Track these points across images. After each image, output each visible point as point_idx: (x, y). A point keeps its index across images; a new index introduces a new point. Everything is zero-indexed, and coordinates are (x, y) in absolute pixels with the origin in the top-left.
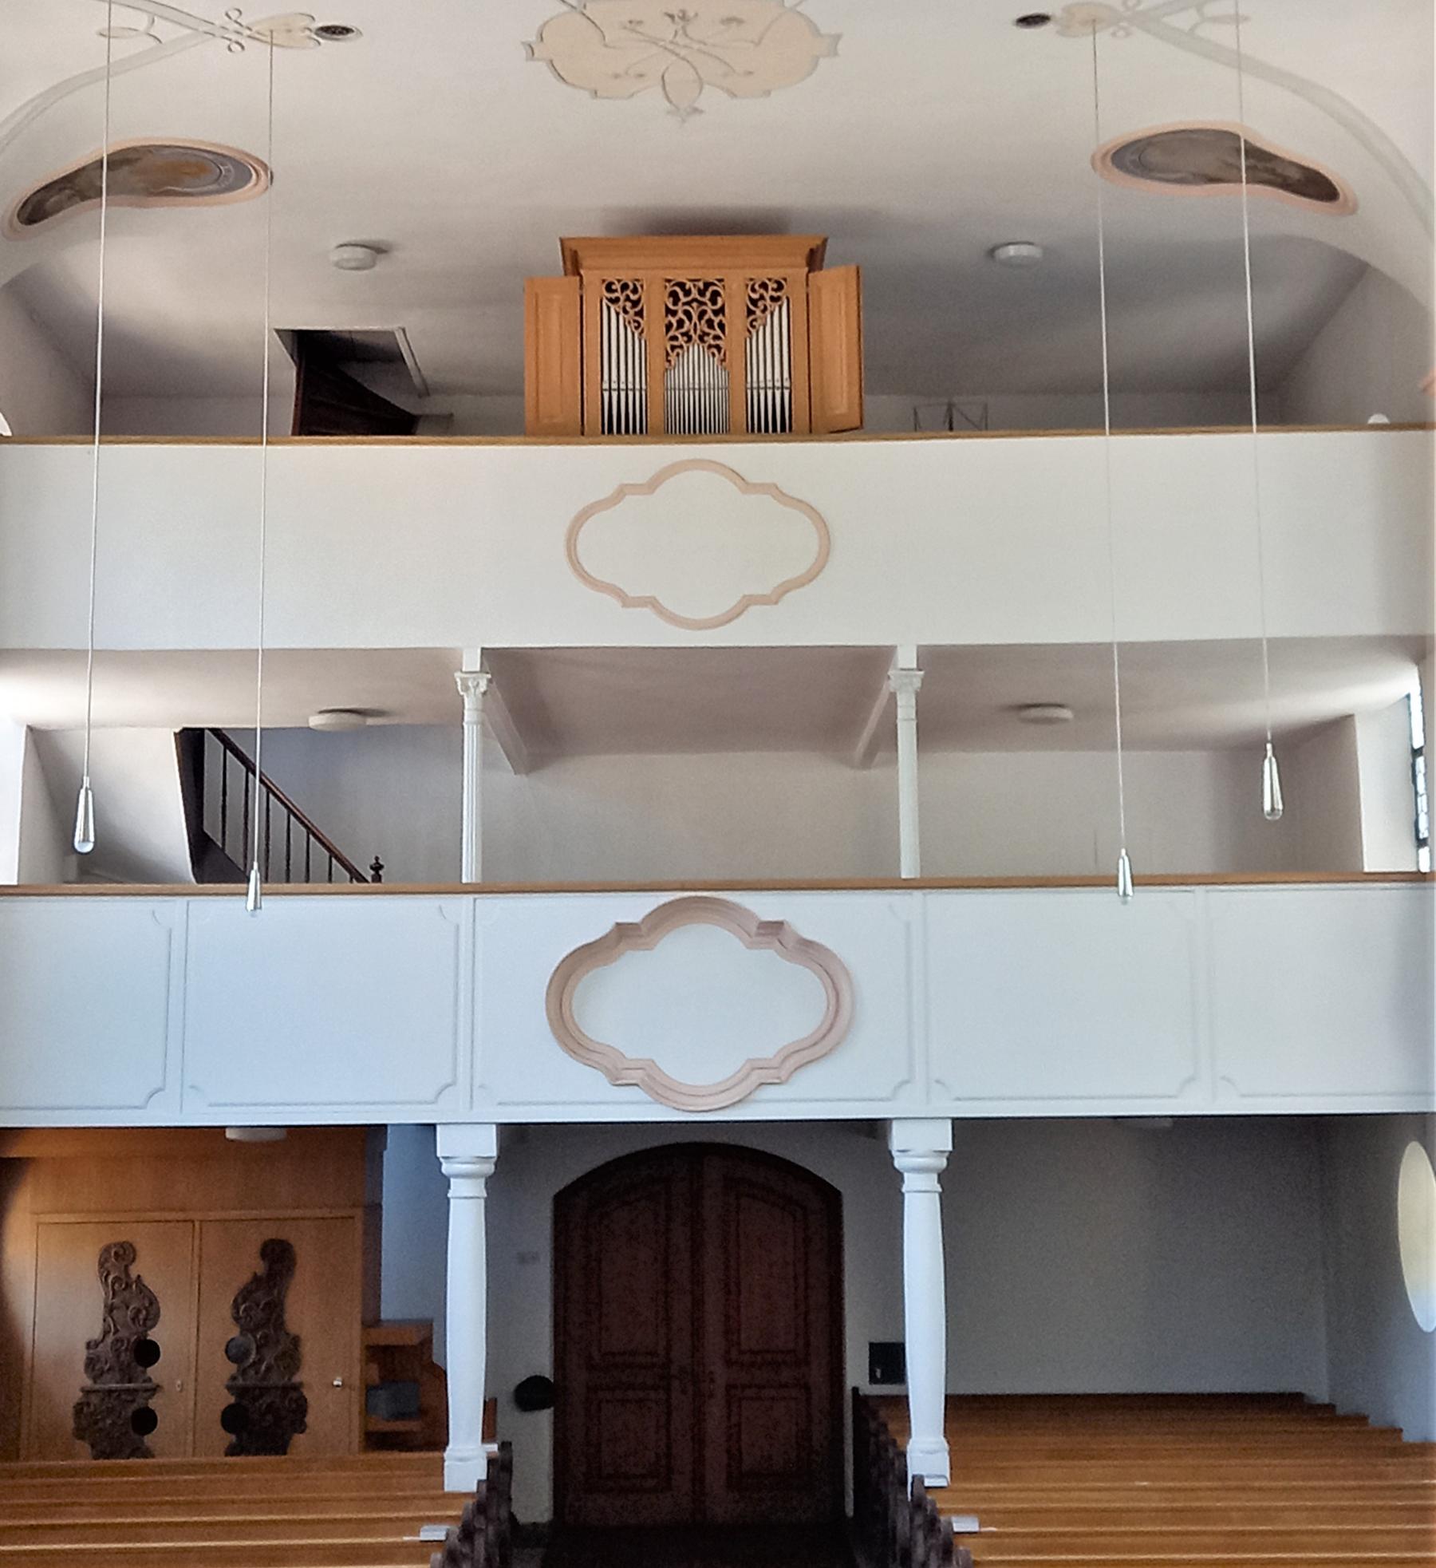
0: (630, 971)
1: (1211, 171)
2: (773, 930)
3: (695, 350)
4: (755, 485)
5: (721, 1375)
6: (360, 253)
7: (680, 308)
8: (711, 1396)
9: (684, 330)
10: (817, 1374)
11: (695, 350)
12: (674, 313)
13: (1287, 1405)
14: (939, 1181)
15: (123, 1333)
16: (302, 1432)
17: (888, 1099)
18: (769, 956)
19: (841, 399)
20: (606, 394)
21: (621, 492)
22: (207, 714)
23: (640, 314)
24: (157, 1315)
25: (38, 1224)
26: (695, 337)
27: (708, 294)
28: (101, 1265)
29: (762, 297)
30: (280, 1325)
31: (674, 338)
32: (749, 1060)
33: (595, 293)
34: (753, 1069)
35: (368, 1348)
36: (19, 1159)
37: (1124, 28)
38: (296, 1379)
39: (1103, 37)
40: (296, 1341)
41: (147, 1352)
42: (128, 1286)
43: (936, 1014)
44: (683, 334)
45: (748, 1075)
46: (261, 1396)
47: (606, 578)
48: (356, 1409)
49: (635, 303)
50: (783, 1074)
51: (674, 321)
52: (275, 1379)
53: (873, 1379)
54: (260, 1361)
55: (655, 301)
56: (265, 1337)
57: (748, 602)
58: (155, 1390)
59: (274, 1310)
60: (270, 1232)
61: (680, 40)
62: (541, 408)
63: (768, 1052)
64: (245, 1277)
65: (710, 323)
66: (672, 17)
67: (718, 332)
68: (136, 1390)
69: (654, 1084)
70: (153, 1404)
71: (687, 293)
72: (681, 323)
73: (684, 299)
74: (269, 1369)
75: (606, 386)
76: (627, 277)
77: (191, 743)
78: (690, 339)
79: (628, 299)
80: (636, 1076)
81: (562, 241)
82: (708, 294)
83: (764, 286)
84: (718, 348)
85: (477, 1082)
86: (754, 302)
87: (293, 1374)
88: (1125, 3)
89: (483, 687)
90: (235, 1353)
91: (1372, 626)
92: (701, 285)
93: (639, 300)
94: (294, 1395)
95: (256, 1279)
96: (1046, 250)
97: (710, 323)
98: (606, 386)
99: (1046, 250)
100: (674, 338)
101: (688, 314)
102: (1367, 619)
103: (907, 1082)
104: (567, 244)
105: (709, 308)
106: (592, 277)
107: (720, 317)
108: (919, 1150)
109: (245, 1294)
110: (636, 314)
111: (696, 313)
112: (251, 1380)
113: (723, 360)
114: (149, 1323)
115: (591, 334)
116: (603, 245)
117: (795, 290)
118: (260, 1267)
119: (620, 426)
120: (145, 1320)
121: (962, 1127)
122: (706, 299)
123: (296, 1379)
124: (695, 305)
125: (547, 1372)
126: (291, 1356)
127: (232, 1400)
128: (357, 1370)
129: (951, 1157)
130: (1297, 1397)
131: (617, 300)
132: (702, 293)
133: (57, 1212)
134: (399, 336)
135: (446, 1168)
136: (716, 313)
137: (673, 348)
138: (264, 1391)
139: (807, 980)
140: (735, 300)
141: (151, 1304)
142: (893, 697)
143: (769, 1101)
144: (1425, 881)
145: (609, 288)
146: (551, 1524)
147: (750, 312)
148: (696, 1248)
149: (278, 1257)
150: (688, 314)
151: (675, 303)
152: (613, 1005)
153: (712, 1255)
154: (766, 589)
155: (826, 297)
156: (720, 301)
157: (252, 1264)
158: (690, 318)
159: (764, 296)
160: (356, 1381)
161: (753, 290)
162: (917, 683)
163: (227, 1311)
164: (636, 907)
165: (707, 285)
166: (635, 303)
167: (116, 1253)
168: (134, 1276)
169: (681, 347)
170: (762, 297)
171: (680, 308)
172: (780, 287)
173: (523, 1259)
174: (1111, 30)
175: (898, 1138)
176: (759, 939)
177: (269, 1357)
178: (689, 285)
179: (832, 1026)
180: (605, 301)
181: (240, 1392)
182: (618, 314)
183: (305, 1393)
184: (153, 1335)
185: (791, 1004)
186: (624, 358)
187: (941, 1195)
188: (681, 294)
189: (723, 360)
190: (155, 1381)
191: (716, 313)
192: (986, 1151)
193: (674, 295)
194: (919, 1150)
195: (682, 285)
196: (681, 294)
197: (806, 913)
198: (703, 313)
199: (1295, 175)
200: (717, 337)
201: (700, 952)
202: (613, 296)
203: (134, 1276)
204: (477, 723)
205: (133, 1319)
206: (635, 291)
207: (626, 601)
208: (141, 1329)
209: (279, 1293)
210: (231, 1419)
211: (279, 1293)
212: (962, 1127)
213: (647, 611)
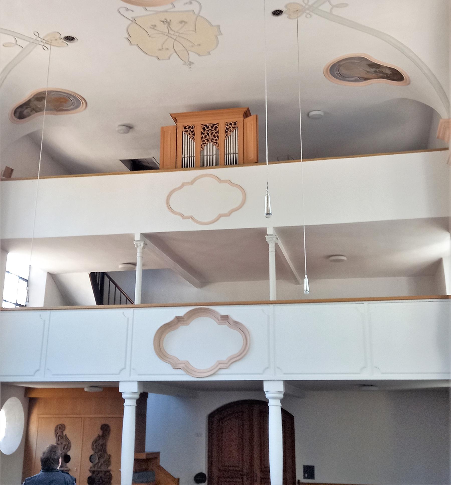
0: (182, 332)
1: (366, 76)
2: (226, 318)
3: (210, 145)
4: (223, 181)
6: (124, 128)
8: (256, 481)
9: (206, 138)
11: (210, 145)
12: (203, 134)
14: (281, 403)
18: (225, 327)
19: (252, 154)
20: (183, 159)
21: (183, 185)
22: (99, 268)
23: (194, 135)
24: (70, 447)
25: (39, 418)
27: (214, 128)
28: (55, 431)
30: (105, 451)
31: (204, 141)
33: (181, 129)
34: (219, 364)
36: (34, 398)
37: (308, 14)
38: (109, 468)
39: (302, 19)
40: (110, 456)
42: (62, 438)
43: (278, 345)
45: (217, 366)
47: (178, 211)
49: (192, 132)
52: (103, 469)
53: (305, 478)
54: (99, 462)
55: (198, 131)
56: (101, 455)
57: (220, 216)
60: (103, 422)
61: (171, 32)
62: (164, 163)
63: (224, 358)
64: (96, 436)
65: (214, 136)
66: (163, 22)
69: (187, 369)
71: (208, 128)
72: (206, 137)
73: (207, 129)
74: (101, 465)
75: (183, 156)
76: (190, 124)
77: (93, 276)
79: (190, 130)
80: (181, 366)
82: (214, 128)
83: (231, 124)
84: (217, 143)
86: (227, 129)
87: (108, 466)
88: (303, 2)
90: (91, 459)
91: (423, 212)
92: (212, 125)
93: (193, 131)
94: (108, 474)
95: (99, 436)
96: (325, 113)
97: (214, 136)
98: (183, 156)
99: (325, 113)
100: (204, 141)
101: (208, 134)
102: (421, 210)
105: (214, 131)
109: (96, 441)
111: (210, 133)
112: (96, 469)
113: (218, 146)
114: (68, 449)
116: (184, 115)
117: (240, 125)
119: (185, 166)
120: (67, 449)
123: (109, 468)
127: (90, 474)
129: (285, 395)
131: (187, 131)
133: (45, 414)
134: (153, 159)
135: (124, 396)
136: (216, 133)
137: (203, 144)
138: (99, 472)
139: (237, 335)
140: (222, 129)
143: (224, 374)
144: (448, 298)
145: (185, 128)
147: (226, 132)
150: (208, 134)
151: (204, 131)
152: (175, 343)
155: (248, 124)
157: (98, 432)
158: (208, 135)
159: (231, 127)
161: (227, 125)
163: (90, 446)
164: (182, 312)
165: (214, 125)
166: (192, 132)
167: (60, 428)
170: (230, 127)
171: (205, 132)
172: (235, 124)
174: (305, 14)
175: (266, 387)
176: (223, 321)
177: (102, 461)
178: (208, 125)
179: (245, 349)
183: (112, 473)
184: (69, 453)
185: (232, 342)
186: (189, 147)
189: (218, 146)
191: (216, 133)
192: (297, 390)
193: (204, 129)
194: (274, 393)
195: (206, 126)
197: (235, 313)
199: (389, 72)
200: (216, 140)
201: (203, 325)
203: (64, 434)
206: (192, 128)
208: (66, 451)
212: (287, 383)
213: (190, 220)
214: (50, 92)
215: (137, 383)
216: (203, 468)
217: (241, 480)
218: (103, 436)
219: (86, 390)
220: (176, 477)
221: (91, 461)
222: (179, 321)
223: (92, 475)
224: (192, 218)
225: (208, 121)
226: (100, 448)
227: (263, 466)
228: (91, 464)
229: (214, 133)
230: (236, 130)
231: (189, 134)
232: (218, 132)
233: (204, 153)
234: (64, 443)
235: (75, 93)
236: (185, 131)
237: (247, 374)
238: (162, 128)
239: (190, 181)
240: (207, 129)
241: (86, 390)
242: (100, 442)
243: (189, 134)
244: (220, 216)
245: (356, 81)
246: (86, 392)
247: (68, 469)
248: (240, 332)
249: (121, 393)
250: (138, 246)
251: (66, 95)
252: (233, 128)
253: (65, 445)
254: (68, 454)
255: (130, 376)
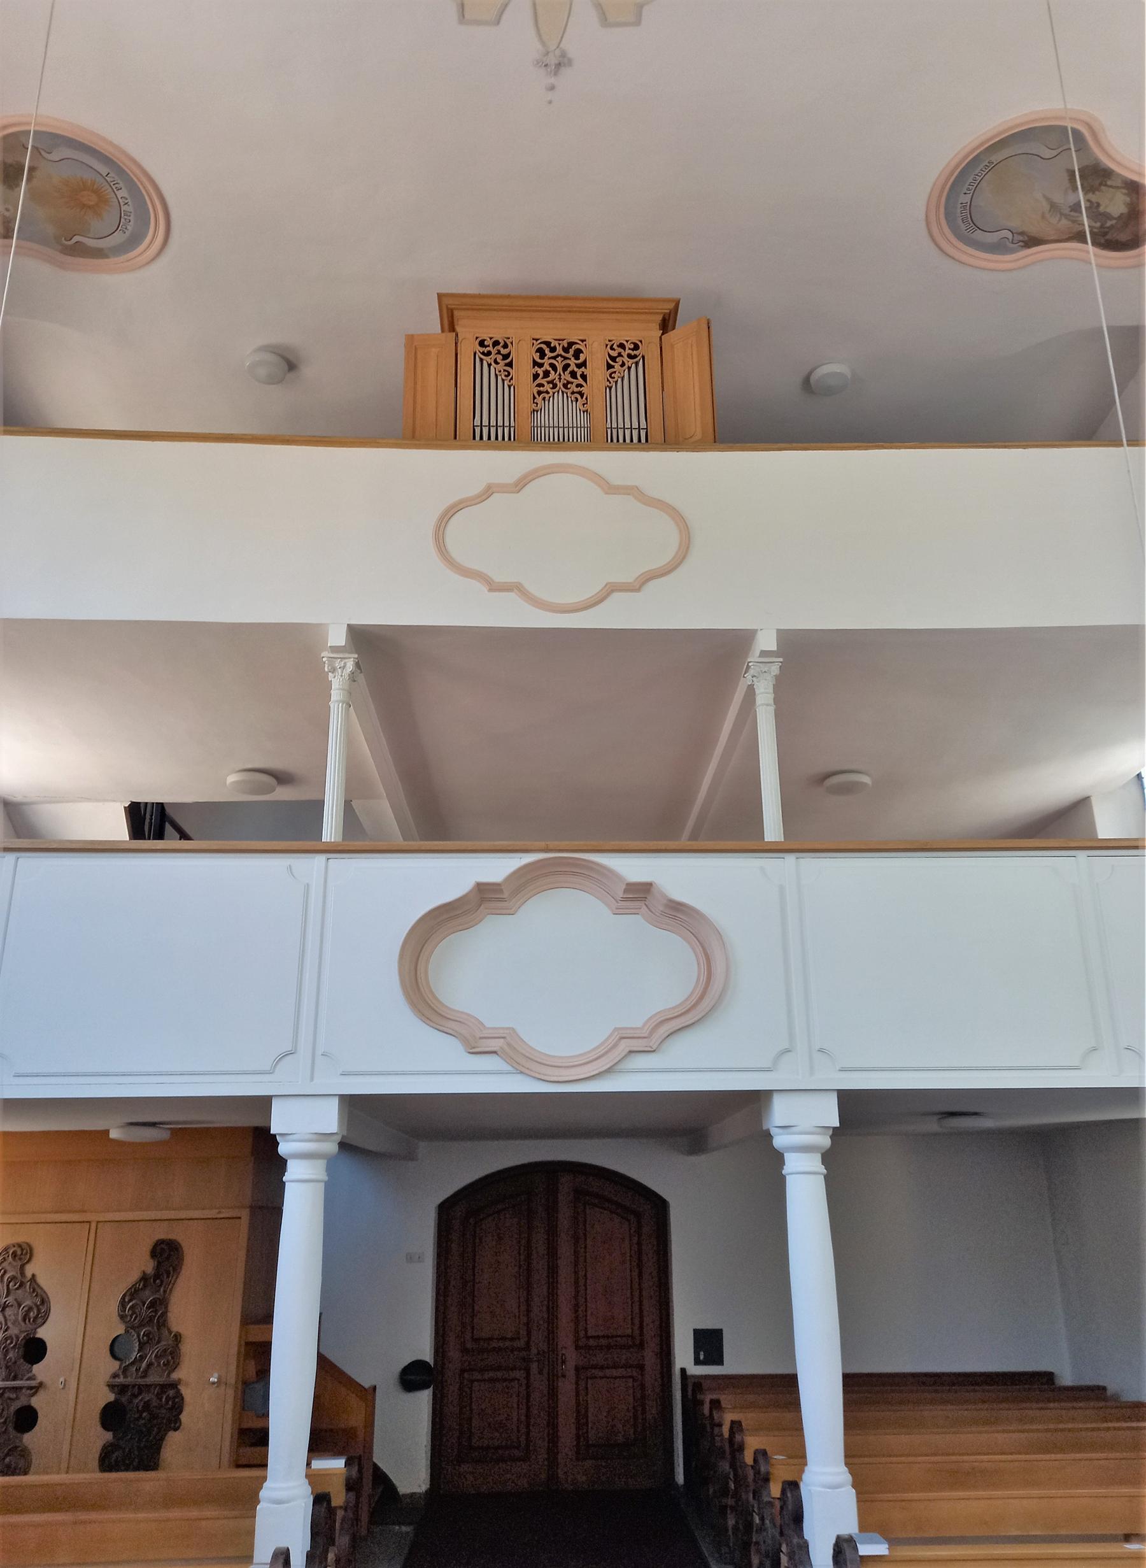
2: (640, 893)
5: (572, 1358)
7: (546, 362)
10: (650, 1358)
12: (541, 365)
13: (1033, 1386)
14: (824, 1162)
15: (14, 1331)
16: (176, 1429)
17: (769, 1070)
18: (635, 924)
20: (478, 430)
21: (488, 492)
23: (510, 365)
26: (560, 385)
27: (572, 351)
29: (620, 355)
30: (163, 1323)
32: (616, 1029)
33: (468, 348)
35: (247, 1344)
38: (175, 1376)
40: (178, 1338)
41: (35, 1350)
42: (22, 1285)
43: (804, 989)
44: (548, 382)
45: (615, 1046)
46: (140, 1393)
48: (229, 1407)
50: (654, 1042)
51: (540, 371)
52: (154, 1378)
53: (697, 1362)
54: (142, 1358)
55: (524, 355)
56: (147, 1335)
57: (612, 589)
58: (36, 1389)
59: (160, 1306)
60: (162, 1233)
63: (637, 1020)
64: (134, 1277)
67: (581, 381)
68: (21, 1388)
69: (512, 1050)
70: (35, 1402)
71: (553, 350)
73: (549, 354)
74: (150, 1365)
76: (498, 337)
78: (555, 386)
79: (499, 352)
80: (494, 1045)
81: (440, 296)
82: (572, 351)
83: (622, 346)
85: (320, 1050)
86: (613, 359)
89: (350, 666)
94: (171, 1393)
95: (144, 1278)
97: (573, 375)
98: (477, 422)
103: (788, 1051)
104: (445, 301)
105: (573, 362)
106: (471, 330)
107: (583, 369)
108: (802, 1126)
110: (506, 365)
111: (560, 365)
114: (40, 1321)
115: (466, 379)
117: (650, 351)
118: (149, 1267)
120: (35, 1318)
121: (849, 1101)
122: (569, 355)
123: (175, 1376)
124: (559, 359)
125: (428, 1356)
126: (172, 1356)
127: (111, 1397)
128: (233, 1368)
129: (836, 1133)
130: (1046, 1379)
131: (489, 353)
132: (566, 350)
135: (283, 1149)
136: (579, 366)
137: (539, 393)
138: (142, 1389)
141: (43, 1302)
142: (751, 691)
145: (482, 344)
146: (430, 1493)
147: (609, 367)
148: (552, 1252)
149: (167, 1255)
152: (471, 971)
153: (565, 1250)
154: (629, 577)
156: (582, 357)
159: (626, 354)
160: (232, 1380)
162: (775, 669)
164: (497, 868)
165: (571, 344)
166: (506, 357)
168: (29, 1275)
169: (548, 392)
170: (620, 355)
171: (546, 362)
172: (636, 347)
173: (410, 1258)
175: (780, 1113)
180: (478, 354)
181: (120, 1389)
182: (489, 365)
183: (184, 1390)
184: (42, 1333)
185: (660, 972)
187: (826, 1177)
188: (547, 351)
190: (40, 1378)
191: (579, 366)
193: (542, 354)
194: (802, 1126)
195: (548, 344)
196: (547, 351)
197: (676, 874)
198: (568, 365)
201: (567, 920)
202: (486, 350)
203: (29, 1275)
204: (343, 702)
205: (24, 1320)
206: (505, 346)
207: (495, 587)
208: (29, 1326)
209: (165, 1292)
210: (111, 1416)
211: (165, 1292)
212: (849, 1101)
213: (512, 595)
214: (51, 140)
215: (335, 1102)
216: (425, 1352)
217: (519, 1374)
218: (157, 1276)
219: (114, 1134)
220: (367, 1385)
221: (114, 1355)
222: (483, 900)
223: (116, 1401)
224: (520, 590)
225: (553, 331)
226: (145, 1312)
227: (582, 1334)
228: (116, 1365)
229: (573, 367)
230: (637, 364)
231: (496, 362)
232: (584, 364)
233: (542, 419)
234: (28, 1303)
235: (139, 166)
236: (483, 353)
237: (730, 1070)
238: (410, 338)
239: (510, 479)
240: (549, 354)
241: (114, 1134)
242: (149, 1296)
243: (496, 362)
244: (612, 589)
245: (998, 248)
246: (113, 1140)
247: (33, 1383)
248: (685, 939)
249: (275, 1136)
250: (334, 670)
251: (104, 170)
252: (630, 356)
253: (30, 1309)
254: (38, 1336)
255: (312, 1079)
